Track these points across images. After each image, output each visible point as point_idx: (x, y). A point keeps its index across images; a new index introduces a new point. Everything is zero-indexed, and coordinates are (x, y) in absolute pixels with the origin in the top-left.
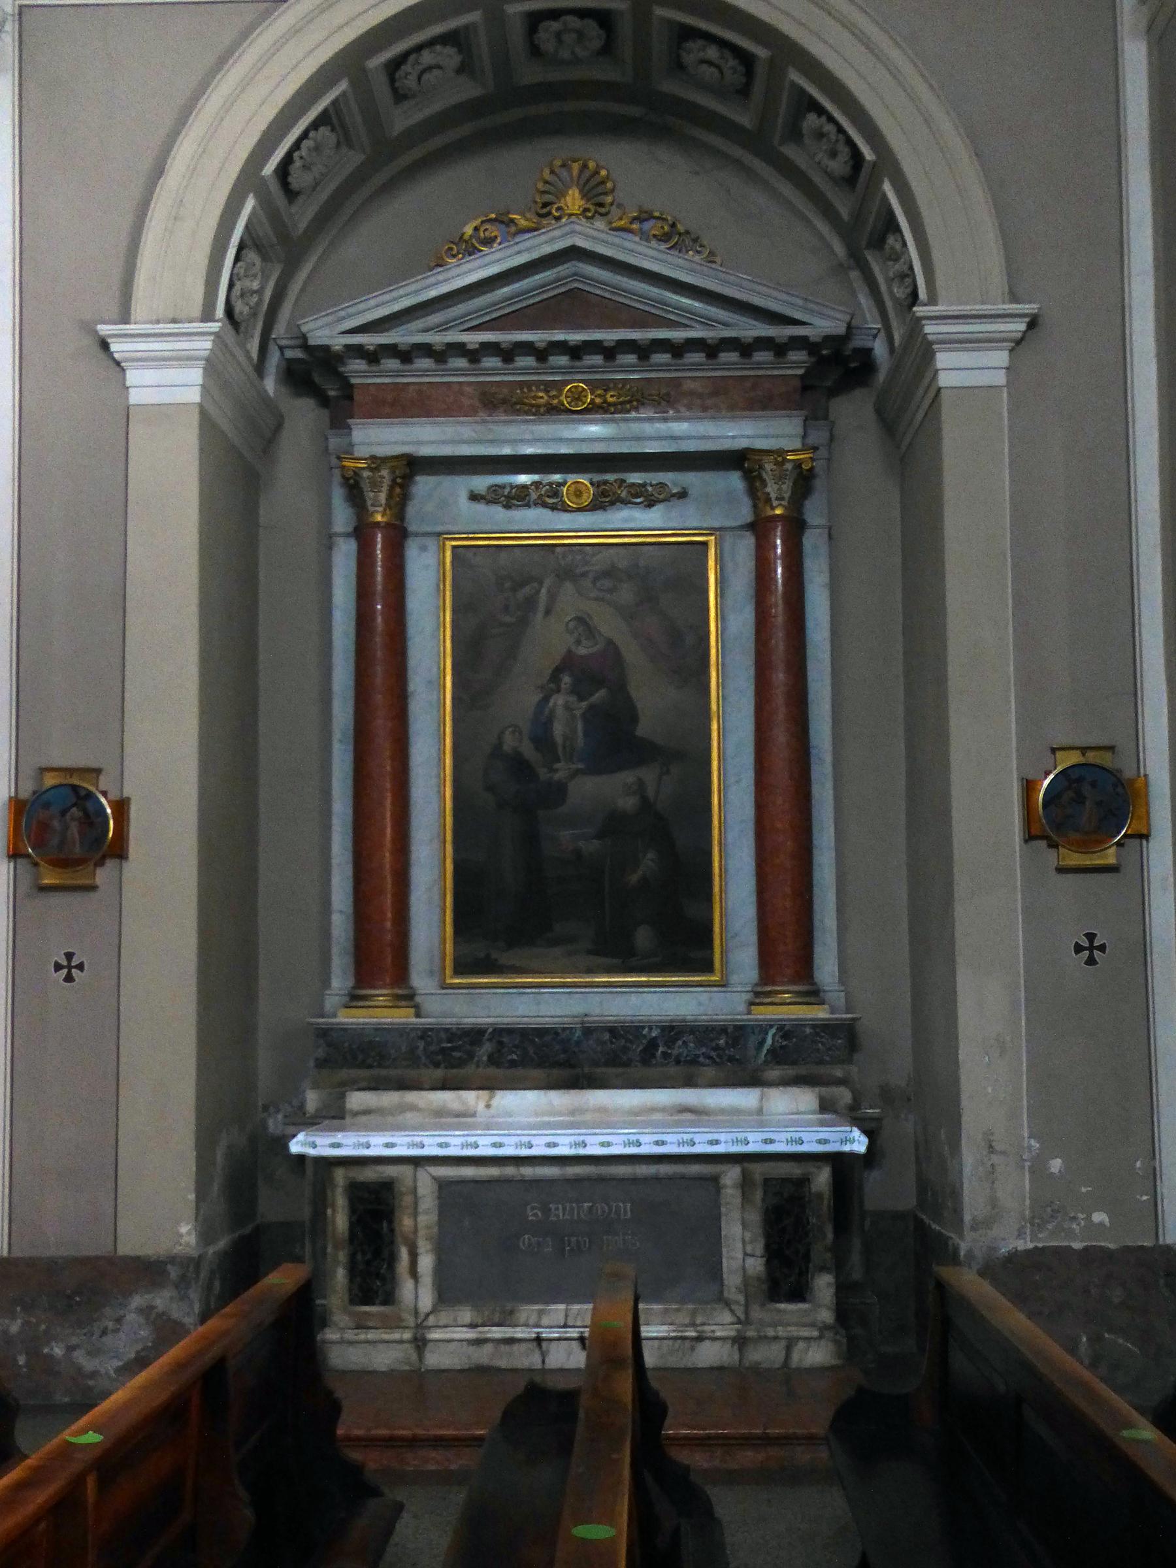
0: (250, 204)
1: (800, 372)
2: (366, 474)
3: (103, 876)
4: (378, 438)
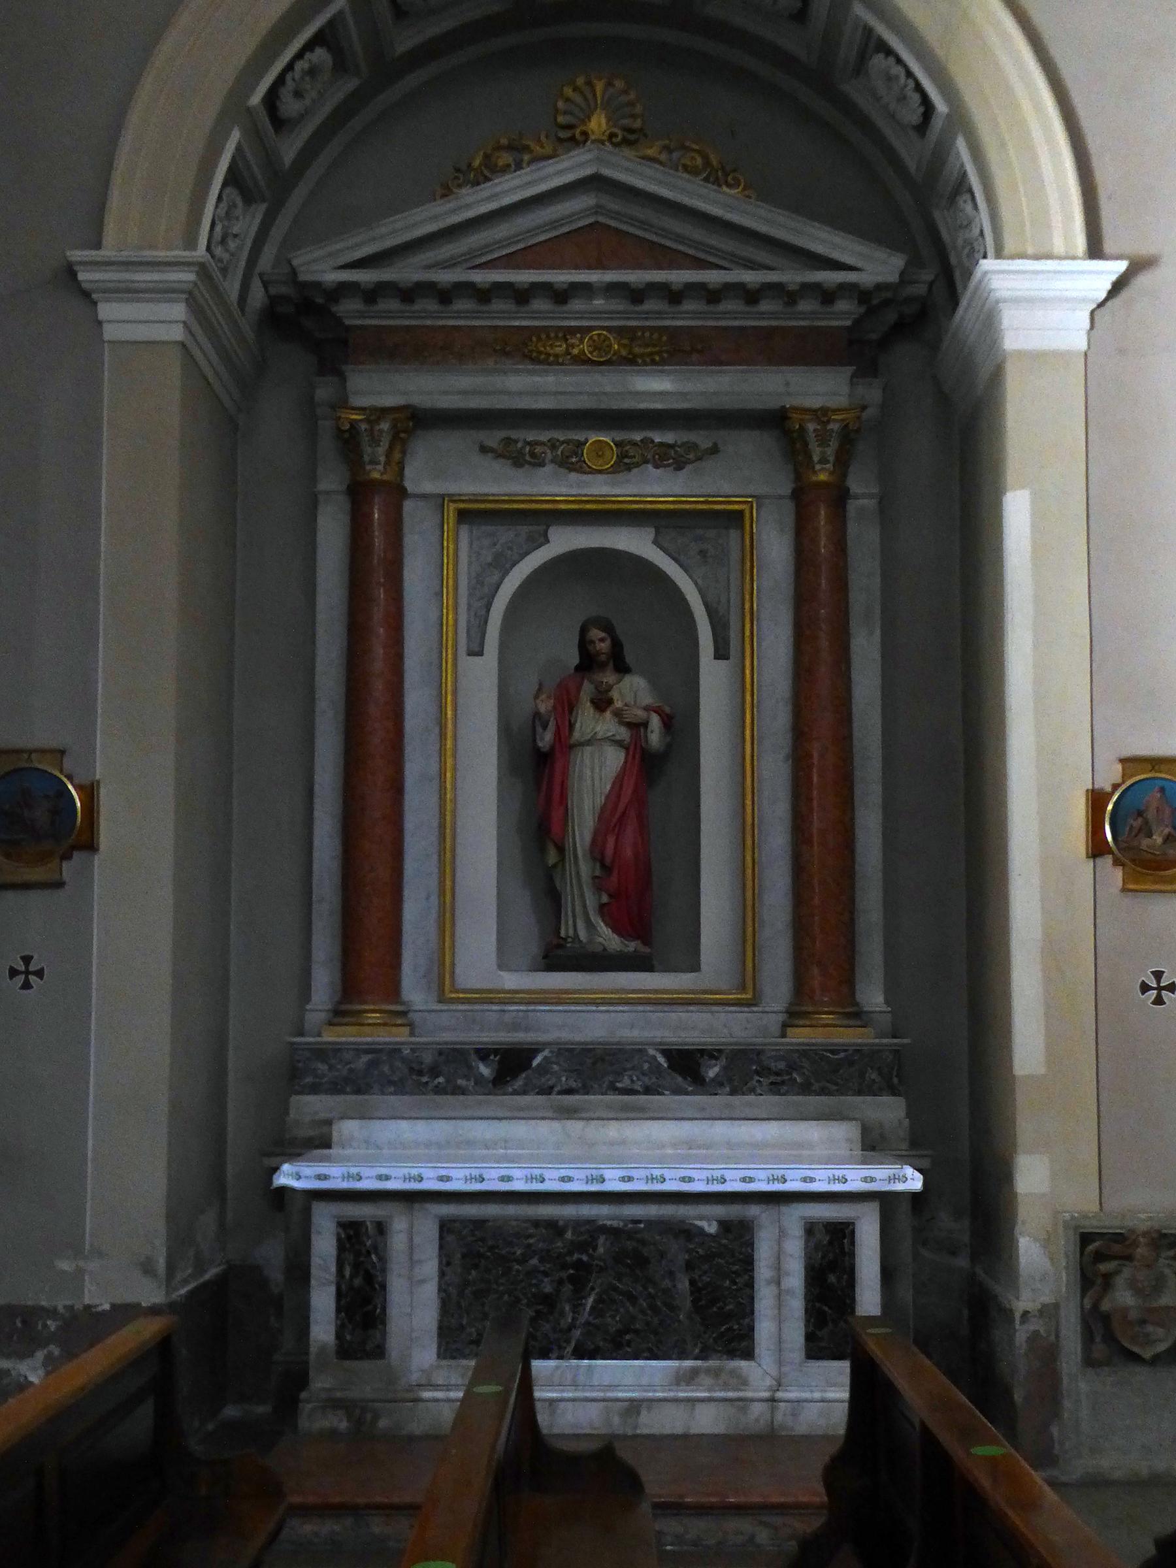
0: (236, 136)
1: (848, 323)
2: (363, 426)
3: (68, 869)
4: (377, 388)
